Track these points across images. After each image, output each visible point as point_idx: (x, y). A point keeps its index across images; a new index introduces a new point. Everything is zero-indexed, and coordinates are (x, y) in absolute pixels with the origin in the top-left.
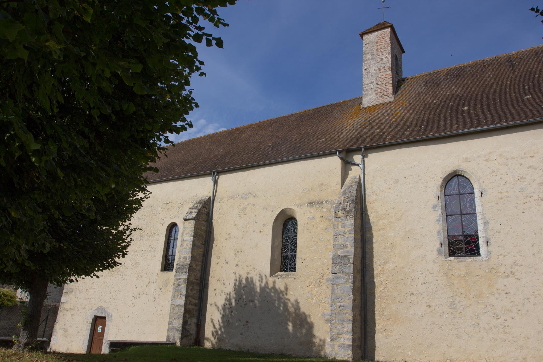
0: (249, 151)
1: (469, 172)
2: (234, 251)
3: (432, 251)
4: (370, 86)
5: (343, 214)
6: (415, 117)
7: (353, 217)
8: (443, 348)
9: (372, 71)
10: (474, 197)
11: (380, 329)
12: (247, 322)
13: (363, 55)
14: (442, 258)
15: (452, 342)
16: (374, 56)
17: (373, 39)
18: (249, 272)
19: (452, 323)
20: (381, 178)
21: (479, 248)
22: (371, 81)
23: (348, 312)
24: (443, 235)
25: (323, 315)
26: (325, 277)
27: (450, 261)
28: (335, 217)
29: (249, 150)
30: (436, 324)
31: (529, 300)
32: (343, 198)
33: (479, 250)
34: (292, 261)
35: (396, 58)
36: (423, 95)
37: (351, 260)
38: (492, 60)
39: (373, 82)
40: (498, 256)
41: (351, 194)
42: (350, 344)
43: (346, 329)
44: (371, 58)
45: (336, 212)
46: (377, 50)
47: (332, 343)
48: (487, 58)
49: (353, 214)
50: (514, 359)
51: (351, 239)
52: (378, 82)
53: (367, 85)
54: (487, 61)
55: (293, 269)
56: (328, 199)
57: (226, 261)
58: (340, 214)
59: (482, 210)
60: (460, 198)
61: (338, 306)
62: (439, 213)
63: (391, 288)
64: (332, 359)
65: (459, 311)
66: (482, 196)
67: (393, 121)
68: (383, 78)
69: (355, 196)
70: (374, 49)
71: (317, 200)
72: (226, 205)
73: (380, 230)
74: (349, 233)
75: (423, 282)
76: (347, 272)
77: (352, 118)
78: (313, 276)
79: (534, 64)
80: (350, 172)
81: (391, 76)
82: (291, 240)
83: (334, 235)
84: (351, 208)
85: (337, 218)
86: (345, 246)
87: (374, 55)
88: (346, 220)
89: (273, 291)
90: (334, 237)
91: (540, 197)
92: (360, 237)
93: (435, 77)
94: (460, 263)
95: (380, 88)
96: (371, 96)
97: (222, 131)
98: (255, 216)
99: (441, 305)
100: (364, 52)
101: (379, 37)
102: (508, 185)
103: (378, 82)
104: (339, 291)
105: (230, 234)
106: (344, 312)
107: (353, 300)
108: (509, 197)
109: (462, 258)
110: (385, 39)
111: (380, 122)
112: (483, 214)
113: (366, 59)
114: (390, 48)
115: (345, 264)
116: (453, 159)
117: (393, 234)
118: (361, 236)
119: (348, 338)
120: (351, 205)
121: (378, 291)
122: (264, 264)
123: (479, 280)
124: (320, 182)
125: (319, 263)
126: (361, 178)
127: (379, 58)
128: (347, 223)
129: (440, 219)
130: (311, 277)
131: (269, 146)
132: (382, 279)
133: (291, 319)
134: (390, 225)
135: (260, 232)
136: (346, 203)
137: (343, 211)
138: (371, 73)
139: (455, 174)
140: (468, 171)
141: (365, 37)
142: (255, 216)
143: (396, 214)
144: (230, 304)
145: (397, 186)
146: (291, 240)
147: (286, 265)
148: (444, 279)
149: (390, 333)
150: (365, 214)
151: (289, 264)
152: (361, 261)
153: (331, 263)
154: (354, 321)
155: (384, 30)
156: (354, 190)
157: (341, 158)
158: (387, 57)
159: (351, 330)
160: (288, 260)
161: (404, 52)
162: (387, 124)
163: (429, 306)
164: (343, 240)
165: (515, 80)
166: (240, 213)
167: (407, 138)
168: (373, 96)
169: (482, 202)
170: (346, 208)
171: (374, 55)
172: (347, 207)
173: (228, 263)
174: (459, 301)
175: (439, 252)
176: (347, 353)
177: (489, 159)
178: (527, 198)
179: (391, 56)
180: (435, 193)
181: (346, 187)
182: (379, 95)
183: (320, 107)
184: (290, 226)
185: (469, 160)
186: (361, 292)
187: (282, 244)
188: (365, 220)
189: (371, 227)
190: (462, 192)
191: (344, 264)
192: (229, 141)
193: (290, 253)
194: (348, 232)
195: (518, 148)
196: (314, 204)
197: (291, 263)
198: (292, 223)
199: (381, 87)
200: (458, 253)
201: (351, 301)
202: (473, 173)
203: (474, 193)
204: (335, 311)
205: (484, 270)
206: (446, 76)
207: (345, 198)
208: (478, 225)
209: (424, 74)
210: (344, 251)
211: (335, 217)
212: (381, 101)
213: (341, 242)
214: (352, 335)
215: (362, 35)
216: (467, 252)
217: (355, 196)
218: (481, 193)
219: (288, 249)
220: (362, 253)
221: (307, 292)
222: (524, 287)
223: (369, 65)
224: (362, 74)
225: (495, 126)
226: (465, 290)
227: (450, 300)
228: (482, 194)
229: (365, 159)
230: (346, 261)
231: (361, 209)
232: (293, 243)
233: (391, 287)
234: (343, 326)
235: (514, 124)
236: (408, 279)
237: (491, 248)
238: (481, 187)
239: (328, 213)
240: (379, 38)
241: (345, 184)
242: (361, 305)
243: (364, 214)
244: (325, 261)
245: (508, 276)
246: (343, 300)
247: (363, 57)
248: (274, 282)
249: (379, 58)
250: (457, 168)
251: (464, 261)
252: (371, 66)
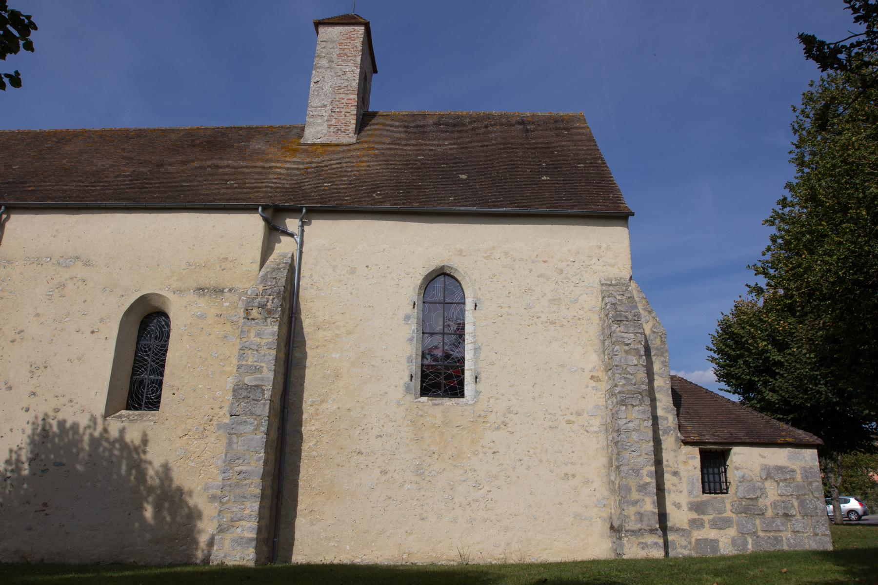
0: (81, 178)
1: (461, 272)
2: (29, 367)
3: (396, 387)
4: (321, 110)
5: (260, 314)
6: (389, 175)
7: (277, 320)
8: (400, 536)
9: (327, 87)
10: (465, 310)
11: (303, 510)
12: (45, 505)
13: (316, 57)
14: (410, 398)
15: (413, 526)
16: (333, 65)
17: (335, 37)
18: (59, 407)
19: (416, 498)
20: (327, 262)
21: (463, 386)
22: (323, 104)
23: (254, 482)
24: (416, 362)
25: (206, 488)
26: (215, 422)
27: (421, 404)
28: (244, 318)
29: (80, 176)
30: (392, 499)
31: (522, 462)
32: (261, 288)
33: (464, 388)
34: (152, 390)
35: (365, 78)
36: (402, 144)
37: (268, 394)
38: (501, 116)
39: (325, 106)
40: (489, 398)
41: (276, 283)
42: (253, 538)
43: (247, 512)
44: (327, 65)
45: (247, 310)
46: (339, 55)
47: (220, 537)
48: (494, 112)
49: (277, 316)
50: (496, 546)
51: (271, 358)
52: (335, 108)
53: (315, 108)
54: (494, 117)
55: (154, 404)
56: (234, 286)
57: (8, 385)
58: (255, 313)
59: (474, 330)
60: (444, 310)
61: (237, 472)
62: (413, 327)
63: (327, 443)
64: (218, 564)
65: (428, 478)
66: (475, 309)
67: (354, 175)
68: (343, 103)
69: (284, 286)
70: (334, 53)
71: (214, 285)
72: (21, 273)
73: (317, 347)
74: (268, 348)
75: (379, 434)
76: (259, 414)
77: (286, 157)
78: (192, 418)
79: (553, 136)
80: (277, 244)
81: (356, 104)
82: (153, 352)
83: (241, 349)
84: (274, 305)
85: (248, 319)
86: (258, 370)
87: (333, 62)
88: (265, 325)
89: (117, 446)
90: (239, 352)
91: (549, 320)
92: (284, 355)
93: (420, 120)
94: (436, 407)
95: (336, 119)
96: (320, 128)
97: (18, 130)
98: (85, 302)
99: (403, 470)
100: (317, 53)
101: (345, 36)
102: (512, 297)
103: (335, 108)
104: (240, 446)
105: (22, 331)
106: (247, 482)
107: (264, 462)
108: (511, 314)
109: (438, 399)
110: (353, 41)
111: (333, 172)
112: (475, 336)
113: (318, 65)
114: (360, 59)
115: (256, 400)
116: (441, 248)
117: (338, 355)
118: (286, 355)
119: (250, 527)
120: (276, 300)
121: (307, 447)
122: (94, 393)
123: (460, 432)
124: (222, 254)
125: (206, 397)
126: (295, 258)
127: (341, 70)
128: (266, 330)
129: (413, 338)
130: (189, 420)
131: (125, 176)
132: (313, 428)
133: (150, 499)
134: (335, 340)
135: (93, 332)
136: (266, 297)
137: (260, 309)
138: (324, 91)
139: (441, 272)
140: (460, 270)
141: (322, 29)
142: (85, 302)
143: (347, 323)
144: (18, 470)
145: (353, 279)
146: (153, 352)
148: (410, 430)
149: (318, 517)
150: (296, 319)
151: (144, 397)
152: (282, 396)
153: (229, 396)
154: (263, 497)
155: (354, 28)
156: (283, 276)
157: (265, 220)
158: (353, 71)
159: (257, 513)
160: (144, 389)
161: (375, 71)
162: (345, 176)
163: (384, 472)
164: (255, 359)
165: (530, 152)
166: (51, 293)
167: (376, 205)
168: (324, 129)
169: (475, 318)
170: (266, 305)
171: (333, 62)
172: (268, 304)
173: (13, 388)
174: (429, 464)
175: (408, 389)
176: (246, 552)
177: (491, 256)
178: (533, 318)
179: (360, 71)
180: (409, 297)
181: (268, 270)
182: (332, 129)
183: (227, 128)
184: (153, 326)
185: (464, 254)
186: (276, 448)
187: (135, 359)
188: (294, 328)
189: (305, 342)
190: (447, 300)
191: (254, 400)
192: (35, 151)
193: (150, 375)
194: (266, 345)
195: (530, 247)
196: (207, 292)
197: (150, 394)
198: (158, 321)
199: (338, 117)
200: (434, 392)
201: (261, 463)
202: (467, 274)
203: (464, 303)
204: (230, 480)
205: (467, 418)
206: (436, 124)
207: (266, 288)
208: (465, 351)
209: (404, 113)
210: (255, 377)
211: (244, 318)
212: (334, 139)
213: (251, 362)
214: (257, 521)
215: (318, 24)
216: (446, 391)
217: (284, 286)
218: (476, 304)
219: (145, 369)
220: (284, 382)
221: (178, 448)
222: (518, 444)
223: (323, 77)
224: (309, 87)
225: (504, 209)
226: (439, 448)
227: (416, 463)
228: (476, 306)
229: (306, 228)
230: (259, 395)
231: (289, 309)
232: (157, 359)
233: (327, 441)
234: (243, 507)
235: (529, 212)
236: (355, 428)
237: (480, 387)
238: (476, 296)
239: (232, 310)
240: (345, 38)
241: (266, 263)
242: (275, 469)
243: (293, 318)
244: (219, 393)
245: (498, 428)
246: (245, 462)
247: (313, 61)
248: (122, 431)
249: (341, 70)
250: (446, 264)
251: (442, 404)
252: (326, 78)
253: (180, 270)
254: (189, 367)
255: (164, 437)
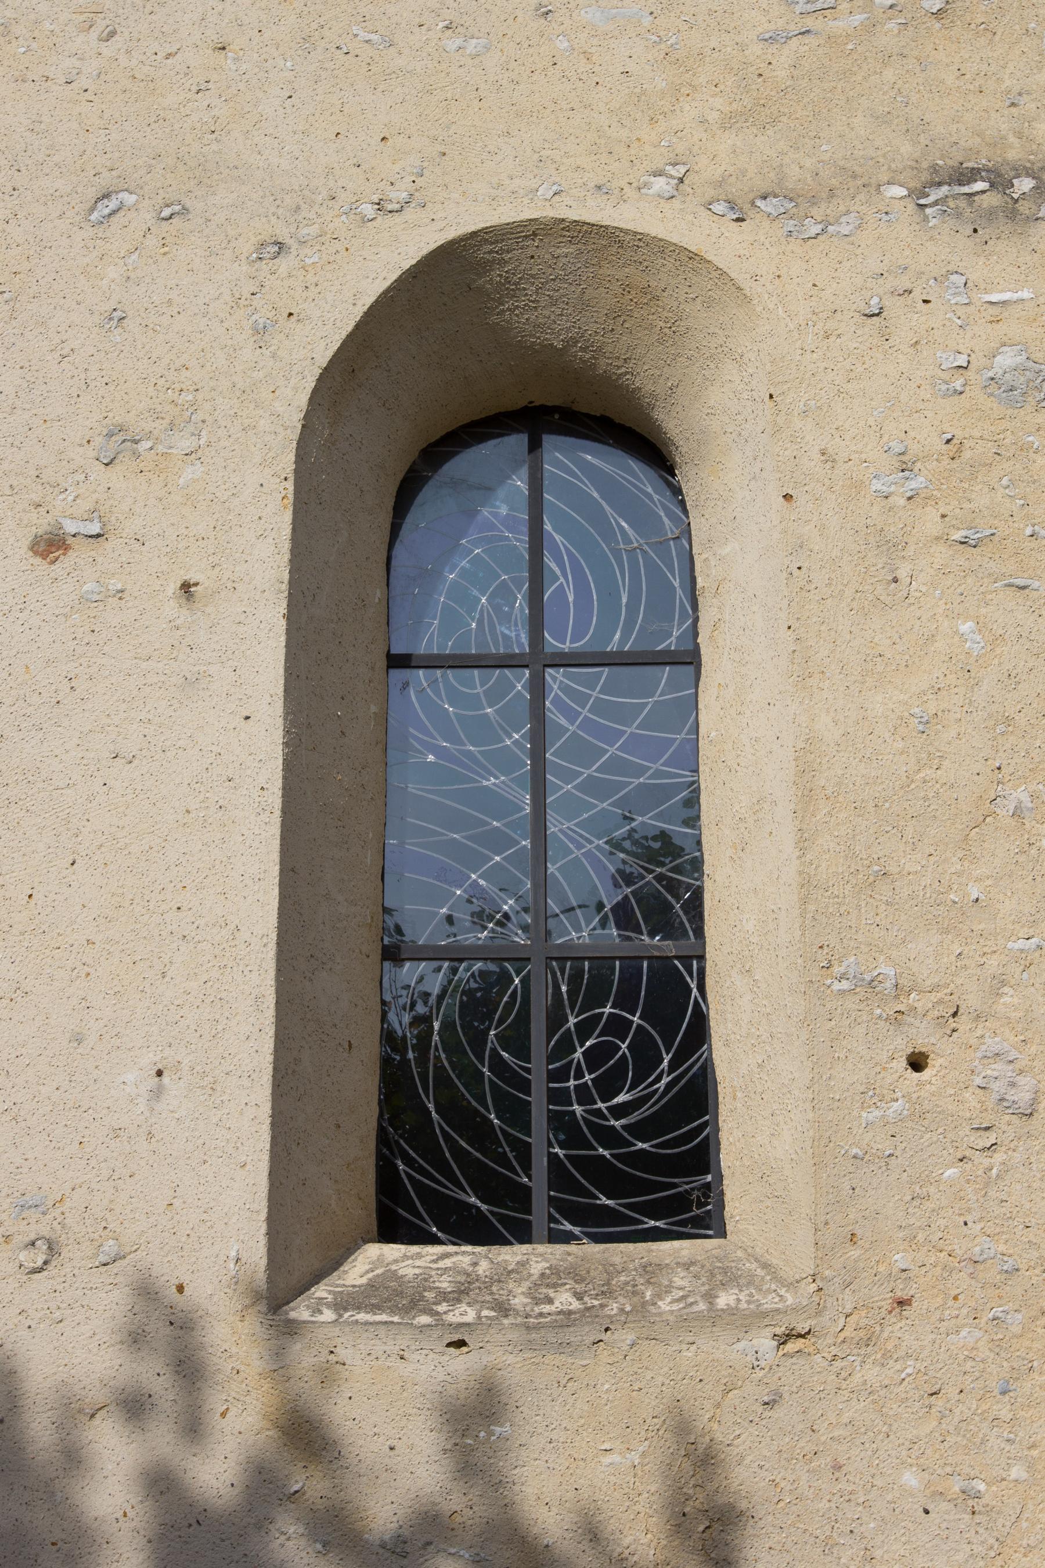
147: (482, 1134)
197: (584, 1095)
253: (742, 47)
254: (1017, 813)
255: (910, 1479)
